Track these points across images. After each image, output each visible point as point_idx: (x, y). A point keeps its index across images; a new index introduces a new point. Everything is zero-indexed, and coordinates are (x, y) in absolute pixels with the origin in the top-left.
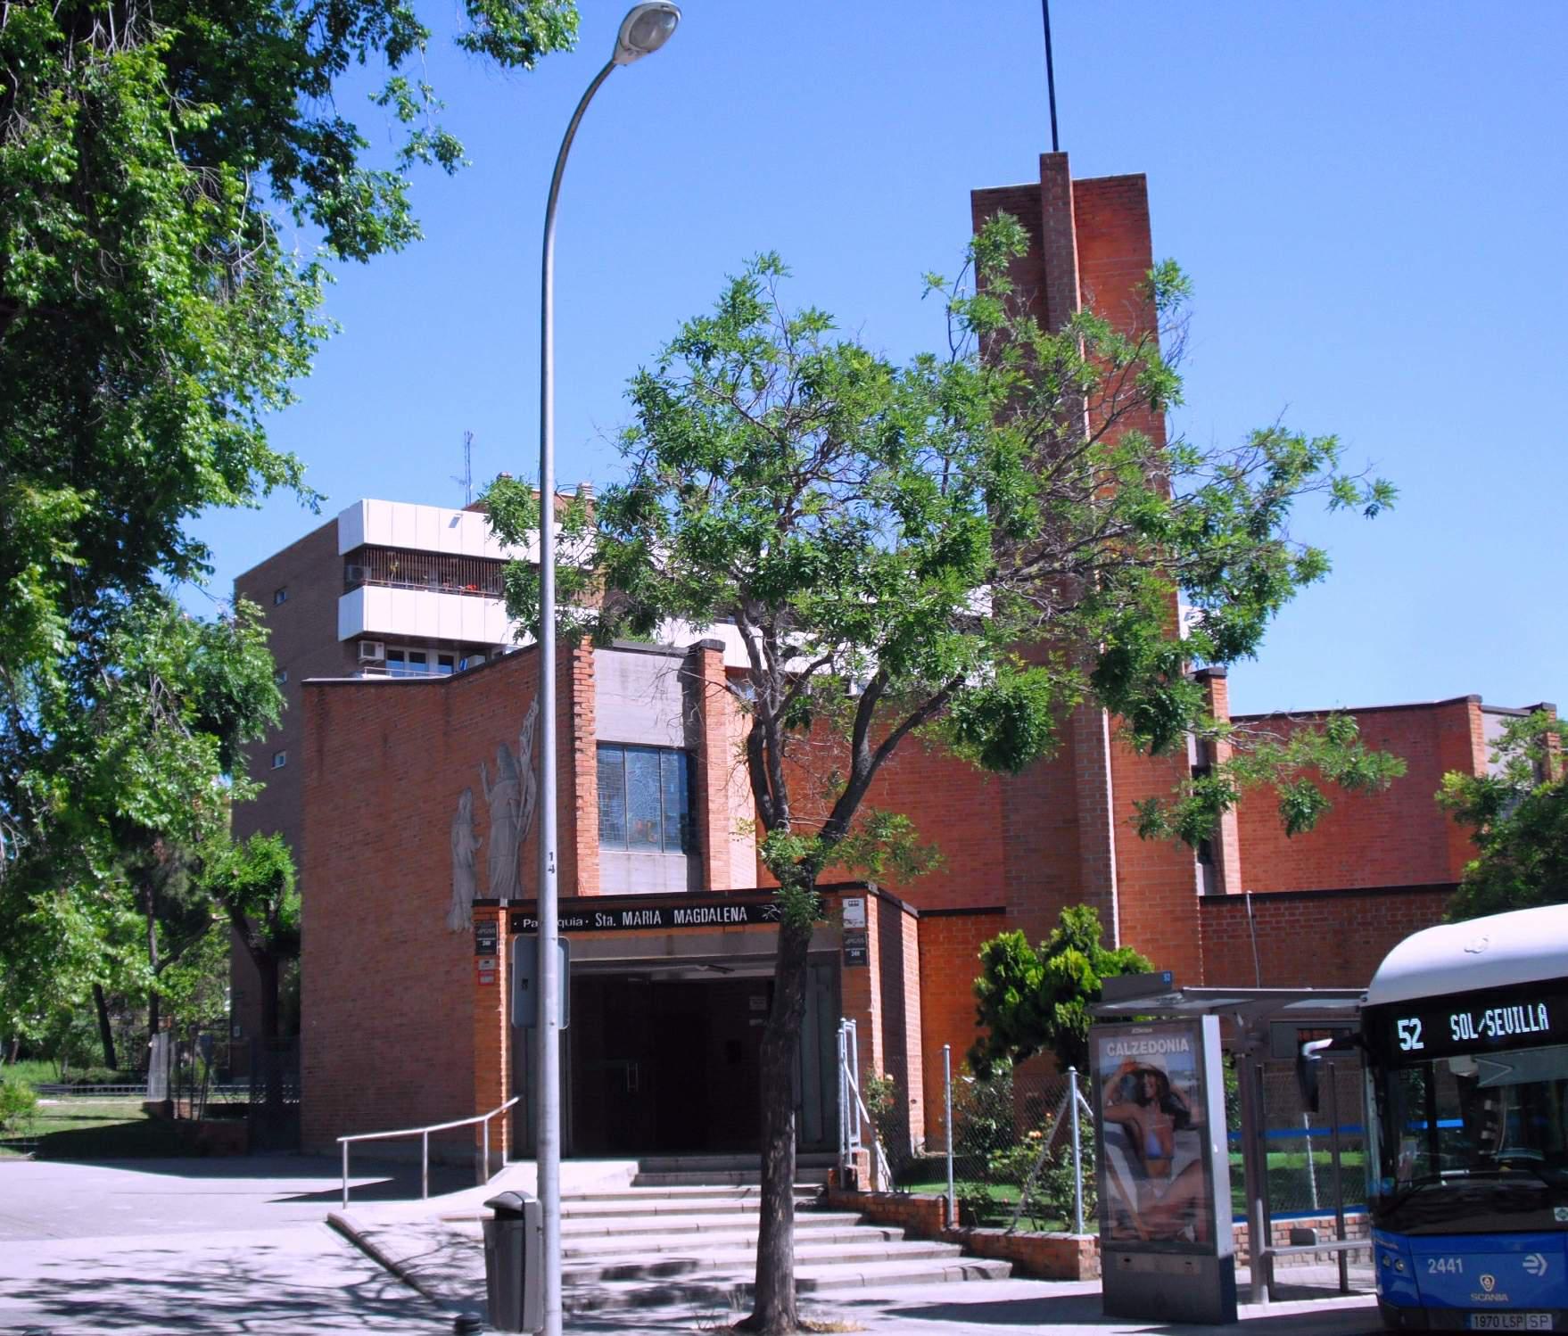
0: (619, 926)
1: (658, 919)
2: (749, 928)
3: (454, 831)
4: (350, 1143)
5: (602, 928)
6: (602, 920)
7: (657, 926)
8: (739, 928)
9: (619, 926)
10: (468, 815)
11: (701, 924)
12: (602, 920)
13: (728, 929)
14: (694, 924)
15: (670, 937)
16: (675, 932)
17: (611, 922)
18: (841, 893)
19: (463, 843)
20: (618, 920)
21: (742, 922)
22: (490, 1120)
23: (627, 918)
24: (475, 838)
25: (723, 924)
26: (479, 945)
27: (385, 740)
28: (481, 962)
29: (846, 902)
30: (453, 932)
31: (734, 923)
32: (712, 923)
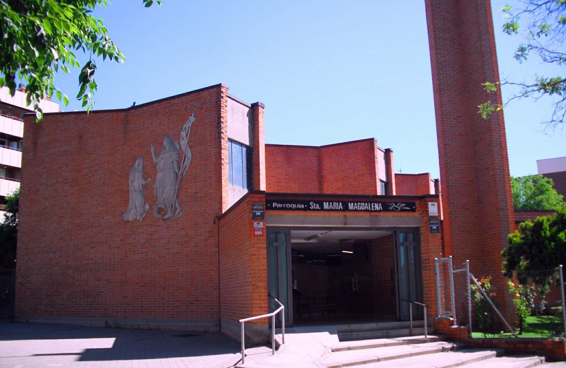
0: (322, 209)
1: (341, 207)
2: (382, 214)
3: (131, 177)
4: (245, 322)
5: (313, 210)
6: (313, 206)
7: (341, 210)
8: (377, 214)
9: (322, 209)
10: (141, 167)
11: (361, 210)
12: (313, 206)
13: (372, 214)
14: (358, 210)
15: (345, 216)
16: (347, 214)
17: (318, 207)
18: (428, 199)
19: (136, 181)
20: (321, 206)
21: (380, 211)
22: (276, 315)
23: (326, 206)
24: (145, 178)
25: (371, 211)
26: (254, 214)
27: (81, 137)
28: (255, 224)
29: (430, 203)
30: (128, 221)
31: (377, 211)
32: (366, 210)
